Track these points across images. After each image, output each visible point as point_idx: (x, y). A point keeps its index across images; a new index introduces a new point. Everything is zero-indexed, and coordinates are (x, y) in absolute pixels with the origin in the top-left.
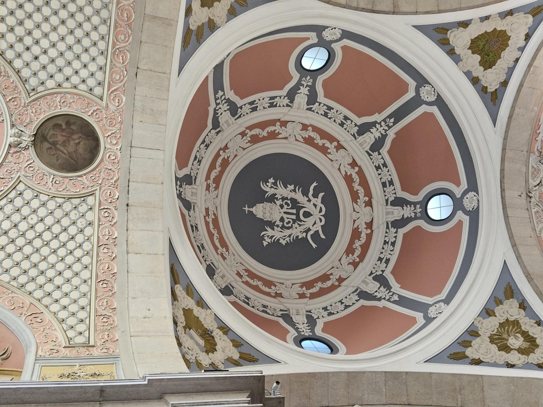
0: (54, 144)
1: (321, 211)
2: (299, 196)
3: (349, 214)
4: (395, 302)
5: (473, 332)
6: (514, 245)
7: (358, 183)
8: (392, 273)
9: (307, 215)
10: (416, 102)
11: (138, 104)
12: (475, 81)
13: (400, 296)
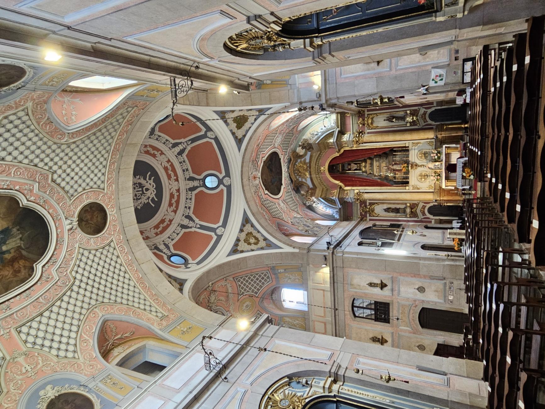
0: (87, 221)
1: (153, 186)
2: (142, 181)
3: (168, 186)
4: (198, 228)
5: (238, 240)
6: (247, 202)
7: (170, 170)
8: (193, 213)
9: (147, 190)
10: (205, 136)
11: (120, 187)
12: (233, 134)
13: (200, 225)
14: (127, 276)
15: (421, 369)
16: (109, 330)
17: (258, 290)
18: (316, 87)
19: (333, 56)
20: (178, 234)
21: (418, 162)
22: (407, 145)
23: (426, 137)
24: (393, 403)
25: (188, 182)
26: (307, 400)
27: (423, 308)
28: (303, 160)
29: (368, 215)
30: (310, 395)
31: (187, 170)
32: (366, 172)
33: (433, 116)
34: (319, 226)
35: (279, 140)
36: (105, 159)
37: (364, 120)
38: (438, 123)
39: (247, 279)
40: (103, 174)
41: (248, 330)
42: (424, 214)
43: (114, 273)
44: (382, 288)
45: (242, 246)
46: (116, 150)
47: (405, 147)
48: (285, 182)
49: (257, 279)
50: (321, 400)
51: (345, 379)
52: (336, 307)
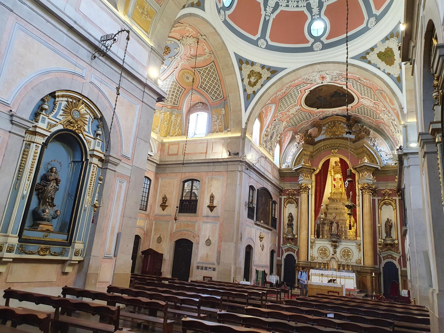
4: (265, 18)
5: (253, 64)
6: (294, 71)
12: (372, 49)
13: (269, 20)
15: (118, 235)
17: (204, 89)
19: (424, 157)
24: (85, 210)
26: (80, 135)
27: (193, 243)
30: (86, 137)
33: (390, 267)
38: (283, 263)
41: (148, 78)
44: (208, 206)
45: (247, 69)
51: (104, 169)
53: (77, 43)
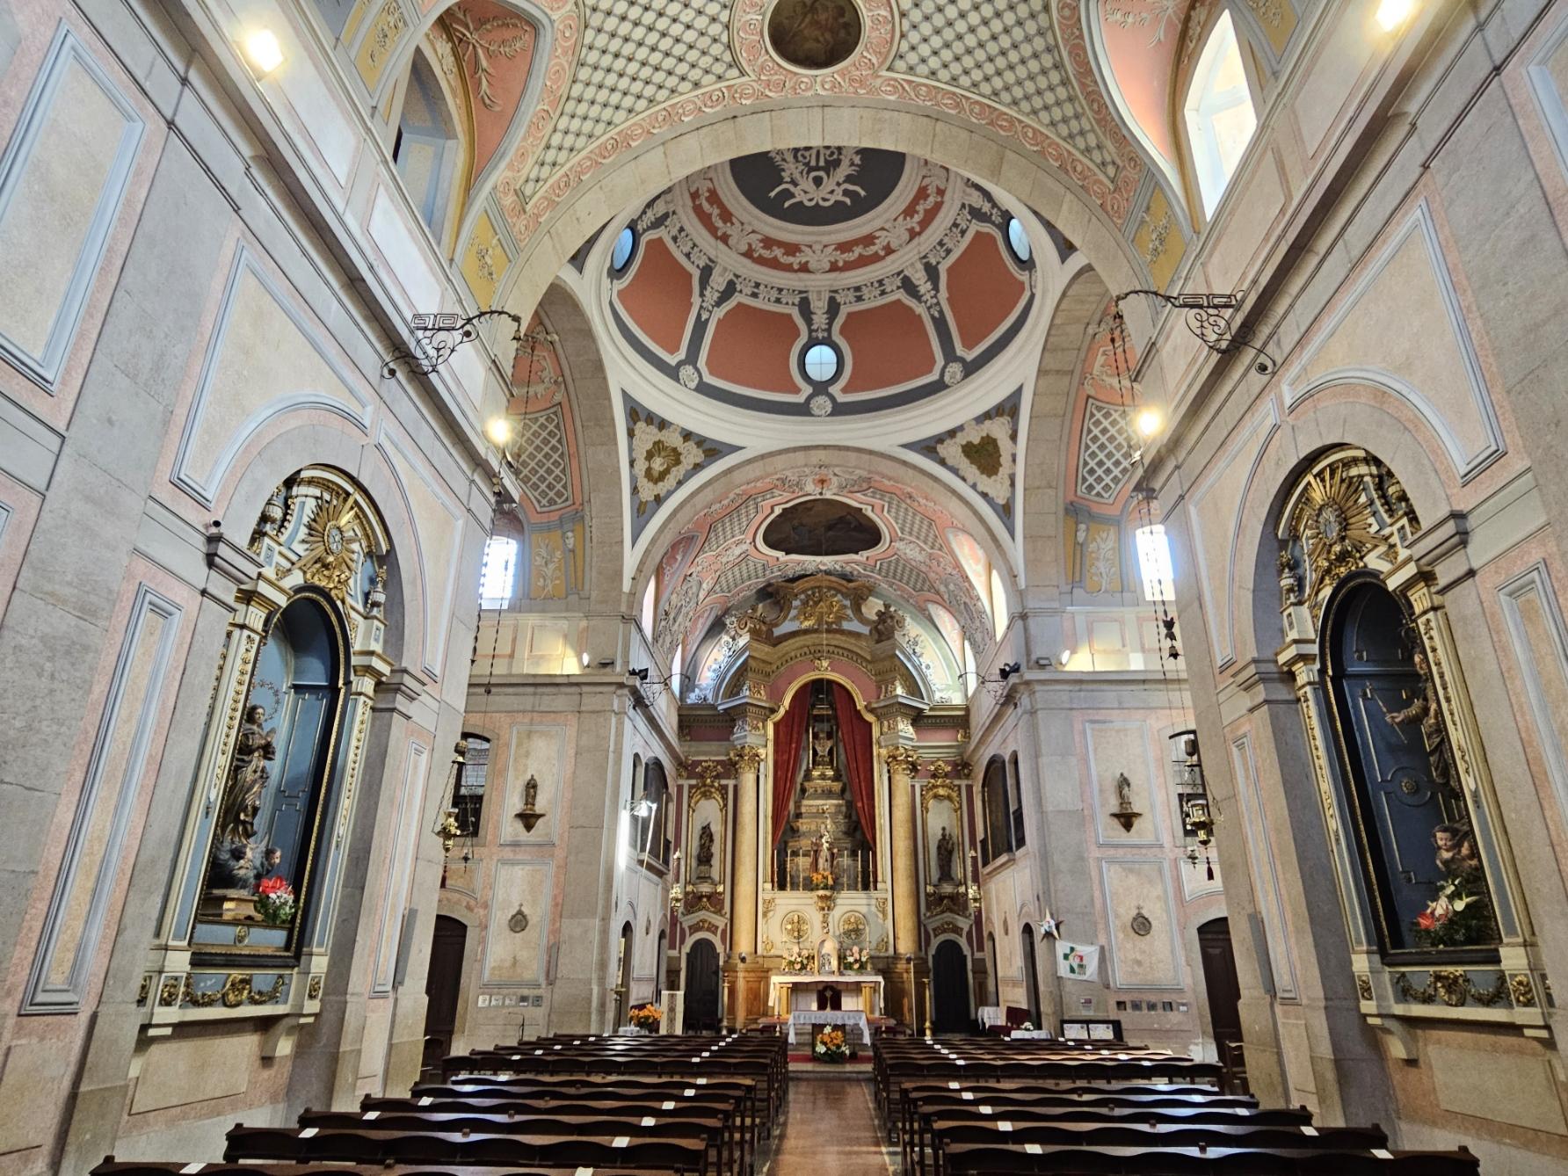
1: (825, 200)
3: (820, 240)
4: (699, 315)
5: (663, 424)
6: (763, 457)
7: (864, 253)
9: (818, 182)
10: (950, 356)
11: (887, 115)
12: (952, 433)
13: (707, 320)
14: (642, 103)
16: (508, 34)
18: (1065, 656)
20: (688, 255)
21: (837, 913)
22: (879, 886)
23: (902, 934)
25: (826, 296)
27: (464, 927)
28: (849, 612)
29: (693, 782)
31: (859, 299)
32: (808, 777)
33: (950, 952)
34: (672, 650)
35: (912, 552)
36: (975, 85)
37: (946, 775)
38: (683, 965)
39: (554, 442)
40: (933, 73)
42: (695, 928)
43: (657, 69)
46: (994, 118)
47: (876, 881)
48: (792, 561)
49: (549, 472)
50: (340, 642)
52: (494, 690)
53: (357, 325)
